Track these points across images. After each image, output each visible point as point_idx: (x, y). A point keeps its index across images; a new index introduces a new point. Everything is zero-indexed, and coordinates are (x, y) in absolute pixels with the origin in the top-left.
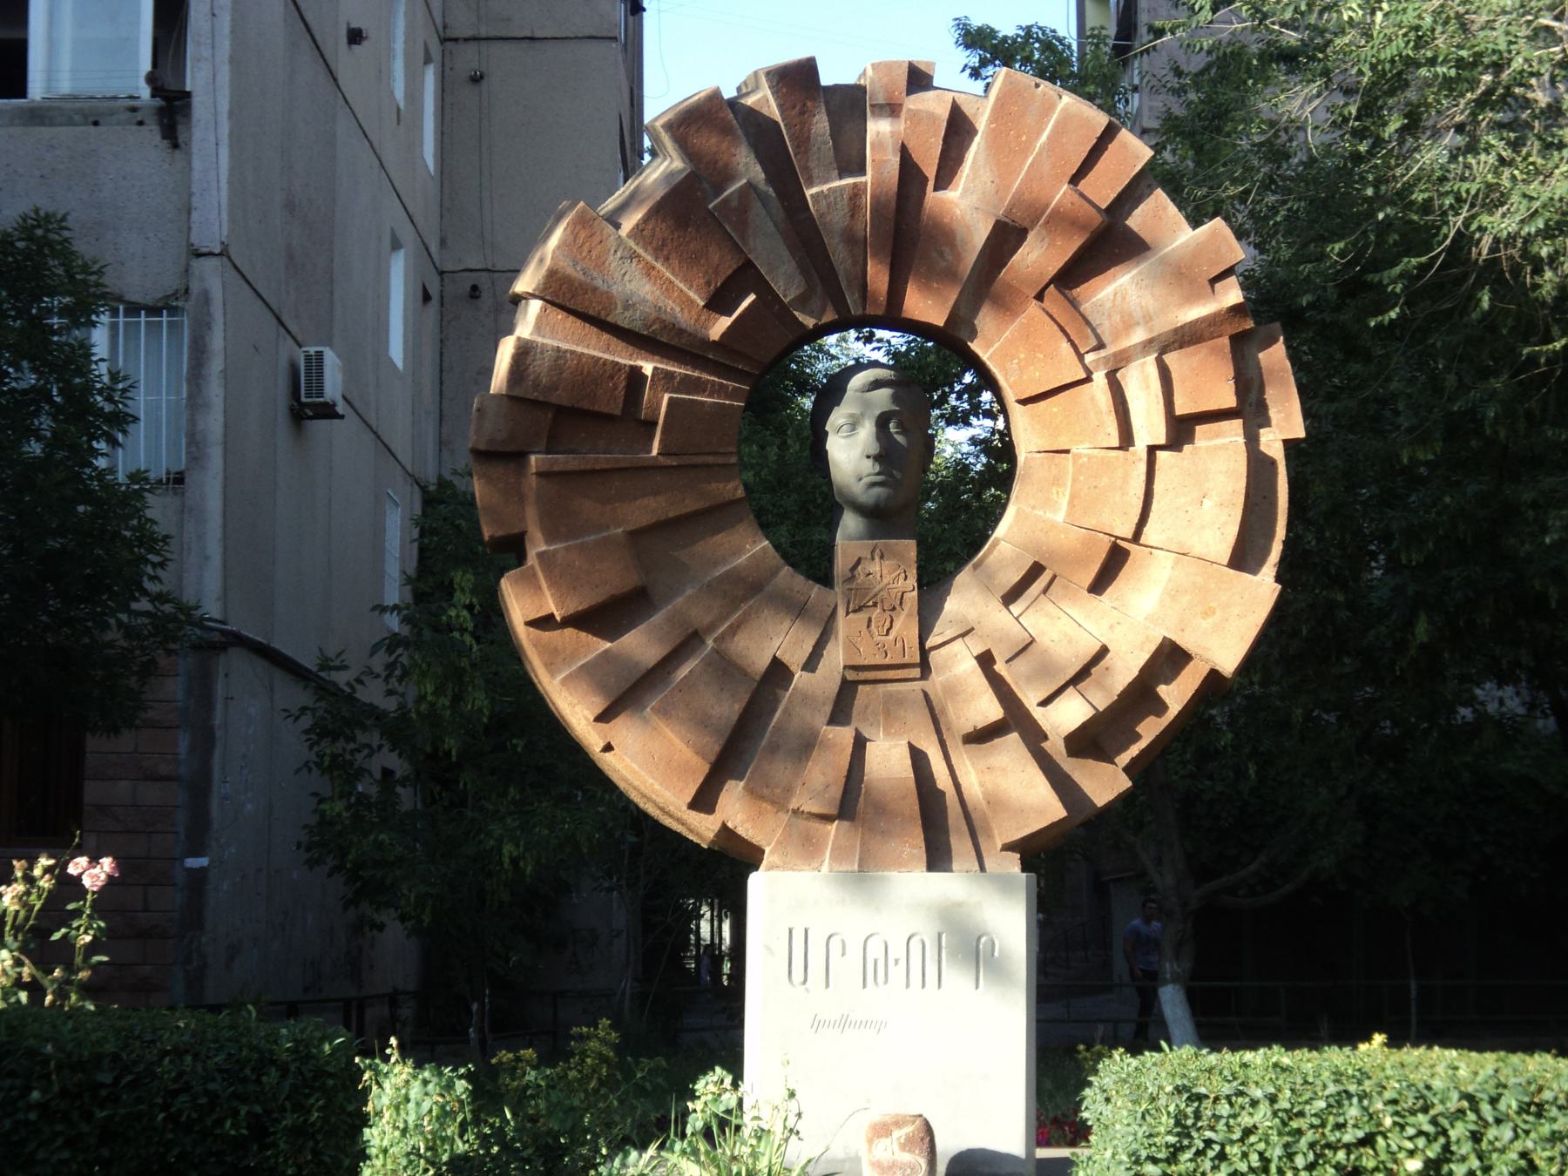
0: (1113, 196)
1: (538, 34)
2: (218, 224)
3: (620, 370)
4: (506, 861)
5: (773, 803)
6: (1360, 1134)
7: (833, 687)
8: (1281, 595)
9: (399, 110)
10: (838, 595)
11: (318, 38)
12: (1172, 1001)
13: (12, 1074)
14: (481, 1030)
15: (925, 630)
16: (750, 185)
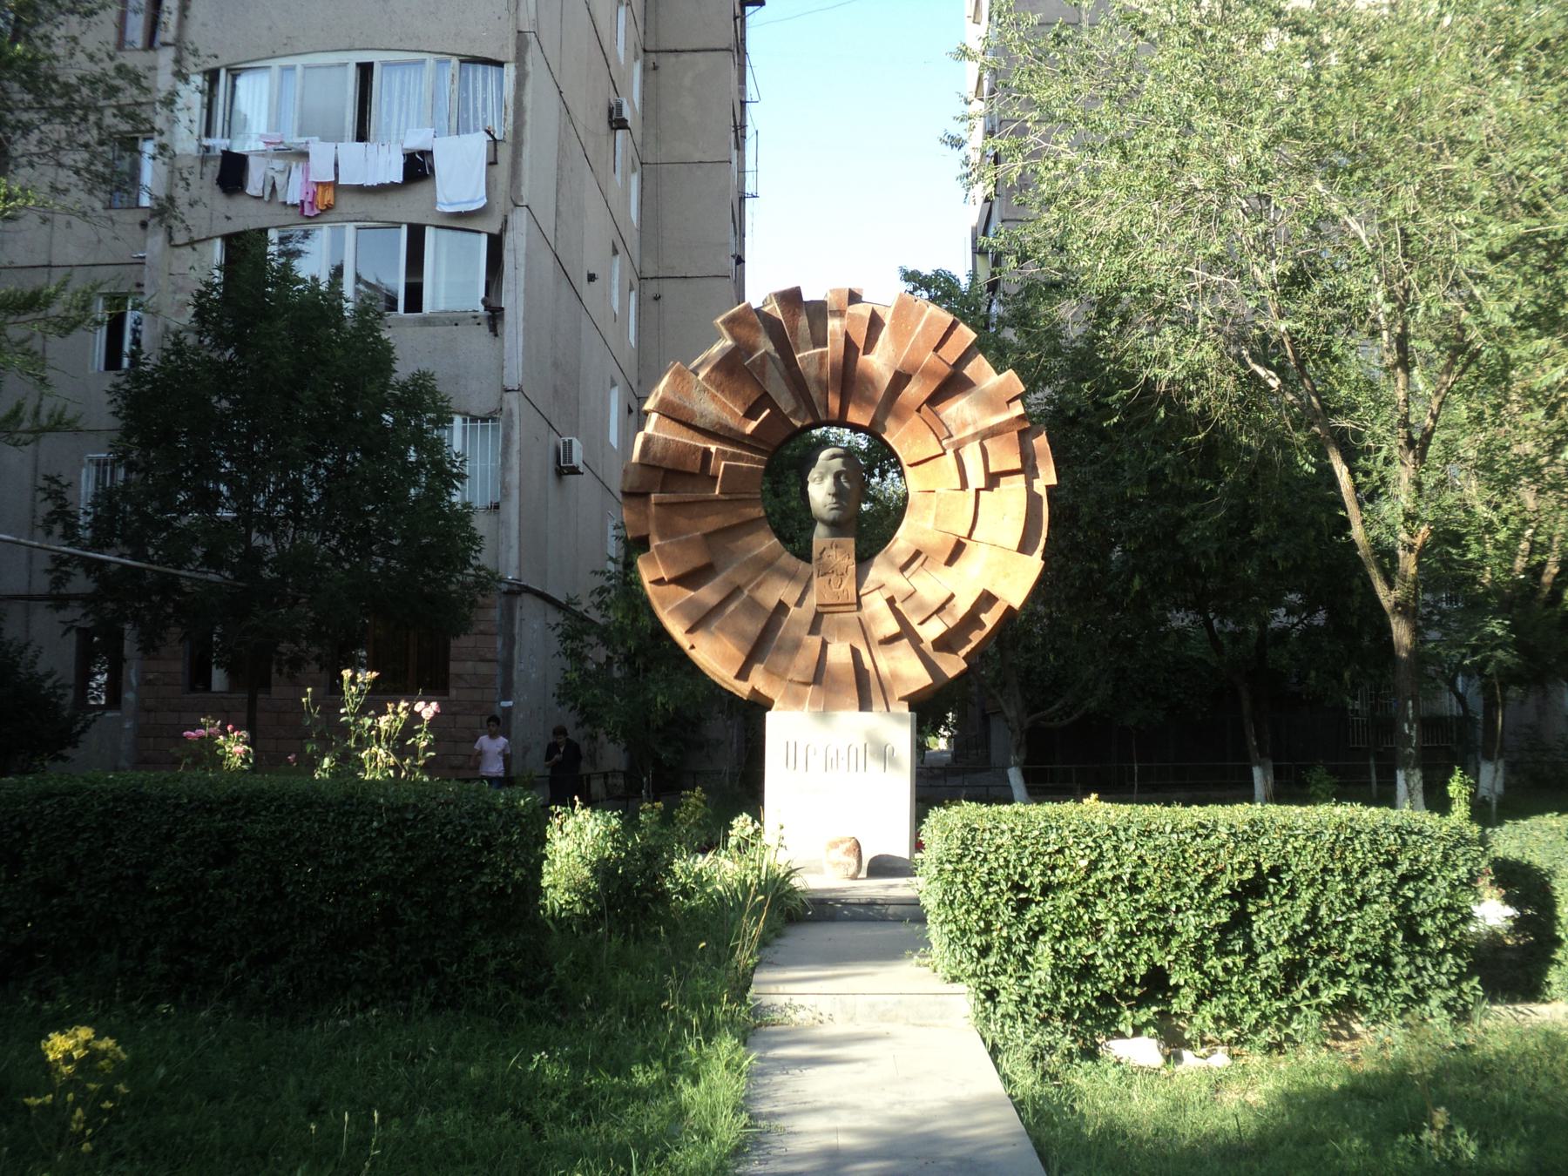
5: (779, 676)
7: (810, 616)
8: (1045, 566)
10: (814, 567)
12: (1015, 776)
13: (364, 813)
14: (648, 792)
15: (859, 585)
16: (766, 352)
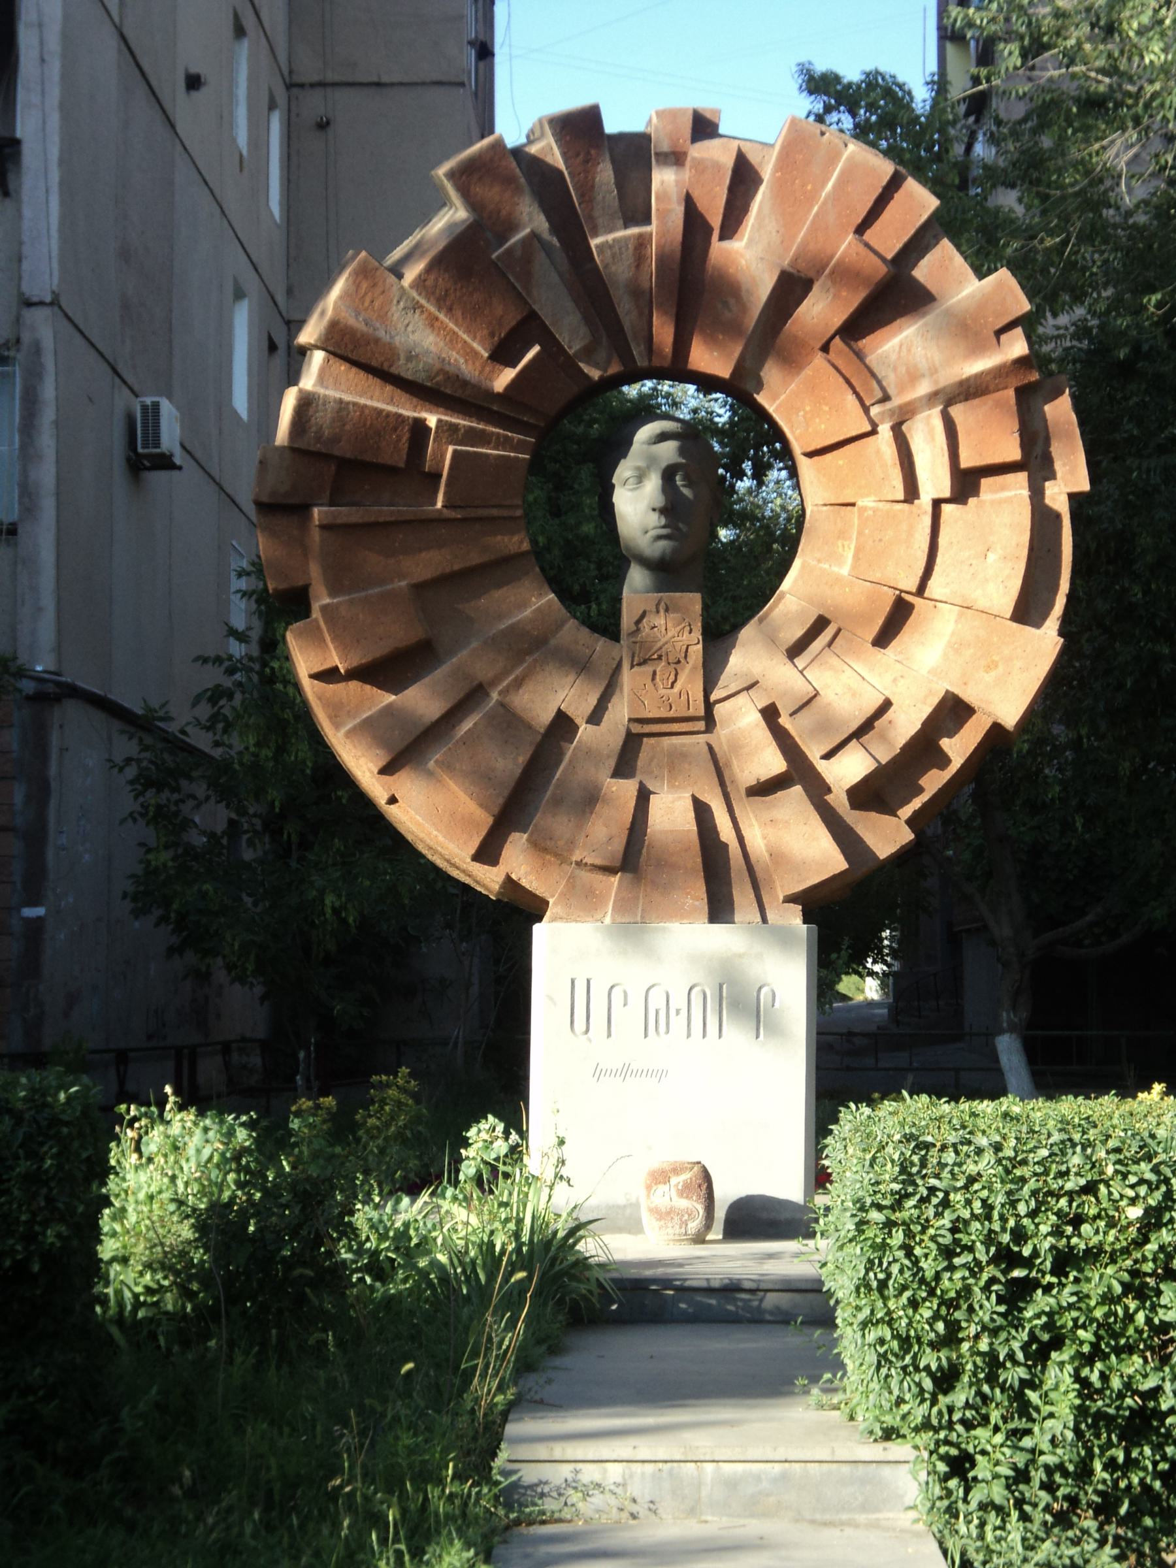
0: (898, 246)
1: (385, 79)
2: (48, 271)
3: (403, 422)
4: (329, 911)
5: (556, 855)
6: (1082, 1182)
7: (617, 741)
9: (241, 155)
10: (622, 650)
11: (154, 83)
15: (709, 684)
16: (534, 235)
